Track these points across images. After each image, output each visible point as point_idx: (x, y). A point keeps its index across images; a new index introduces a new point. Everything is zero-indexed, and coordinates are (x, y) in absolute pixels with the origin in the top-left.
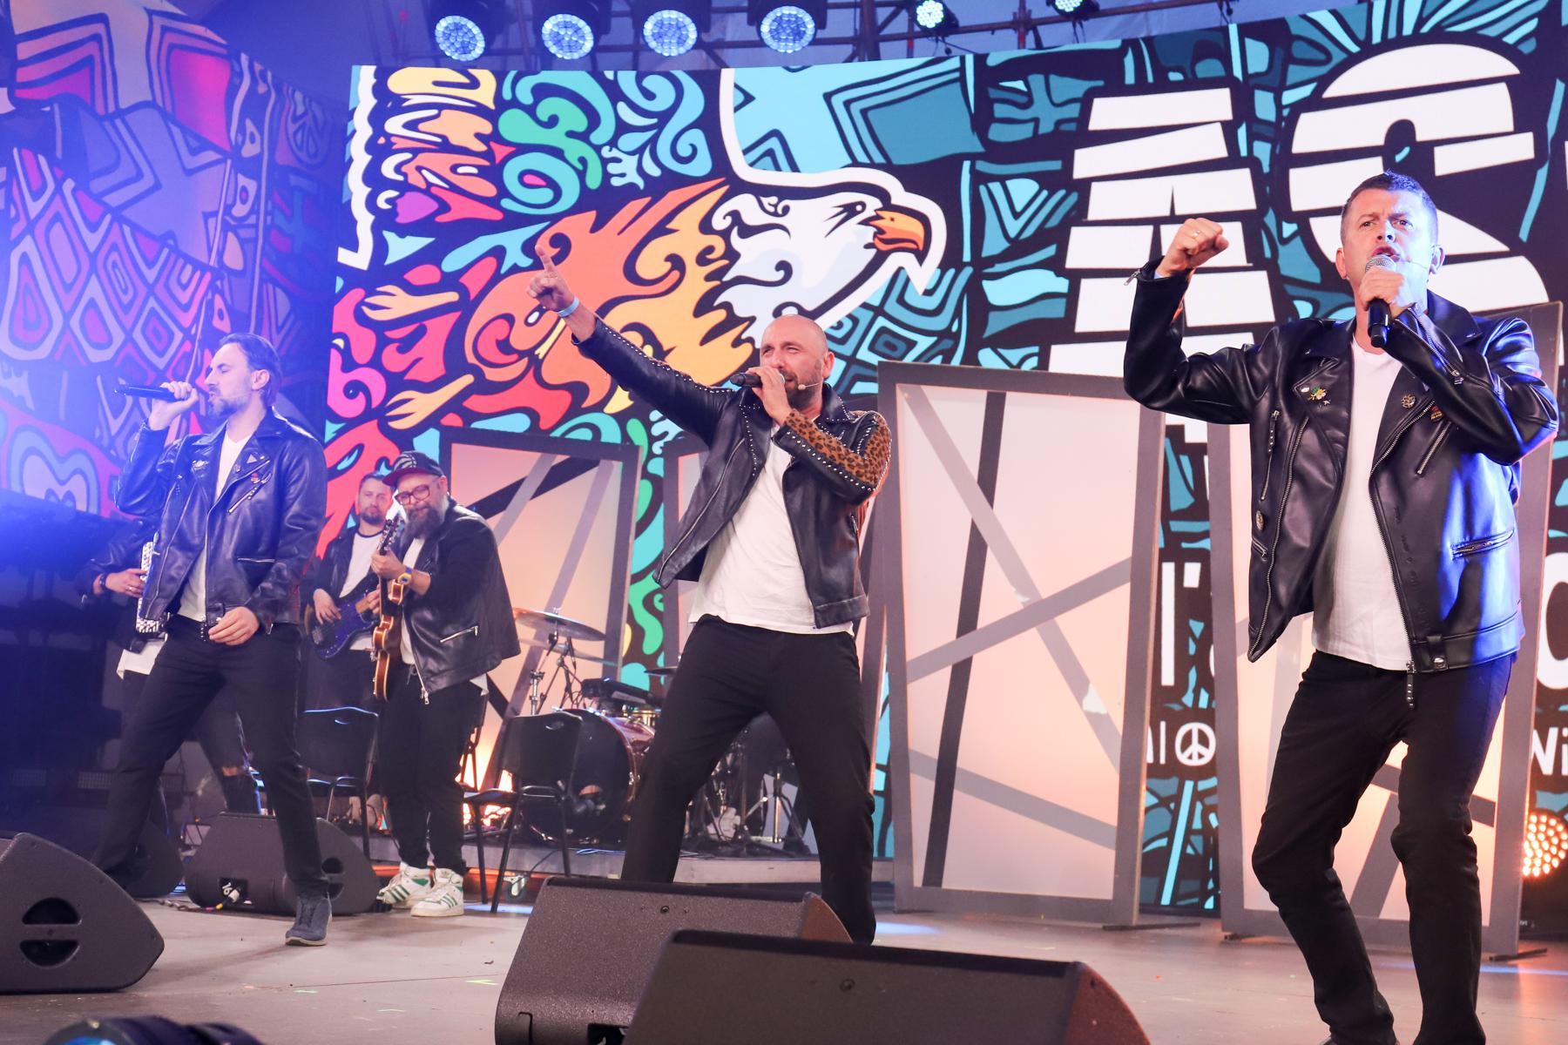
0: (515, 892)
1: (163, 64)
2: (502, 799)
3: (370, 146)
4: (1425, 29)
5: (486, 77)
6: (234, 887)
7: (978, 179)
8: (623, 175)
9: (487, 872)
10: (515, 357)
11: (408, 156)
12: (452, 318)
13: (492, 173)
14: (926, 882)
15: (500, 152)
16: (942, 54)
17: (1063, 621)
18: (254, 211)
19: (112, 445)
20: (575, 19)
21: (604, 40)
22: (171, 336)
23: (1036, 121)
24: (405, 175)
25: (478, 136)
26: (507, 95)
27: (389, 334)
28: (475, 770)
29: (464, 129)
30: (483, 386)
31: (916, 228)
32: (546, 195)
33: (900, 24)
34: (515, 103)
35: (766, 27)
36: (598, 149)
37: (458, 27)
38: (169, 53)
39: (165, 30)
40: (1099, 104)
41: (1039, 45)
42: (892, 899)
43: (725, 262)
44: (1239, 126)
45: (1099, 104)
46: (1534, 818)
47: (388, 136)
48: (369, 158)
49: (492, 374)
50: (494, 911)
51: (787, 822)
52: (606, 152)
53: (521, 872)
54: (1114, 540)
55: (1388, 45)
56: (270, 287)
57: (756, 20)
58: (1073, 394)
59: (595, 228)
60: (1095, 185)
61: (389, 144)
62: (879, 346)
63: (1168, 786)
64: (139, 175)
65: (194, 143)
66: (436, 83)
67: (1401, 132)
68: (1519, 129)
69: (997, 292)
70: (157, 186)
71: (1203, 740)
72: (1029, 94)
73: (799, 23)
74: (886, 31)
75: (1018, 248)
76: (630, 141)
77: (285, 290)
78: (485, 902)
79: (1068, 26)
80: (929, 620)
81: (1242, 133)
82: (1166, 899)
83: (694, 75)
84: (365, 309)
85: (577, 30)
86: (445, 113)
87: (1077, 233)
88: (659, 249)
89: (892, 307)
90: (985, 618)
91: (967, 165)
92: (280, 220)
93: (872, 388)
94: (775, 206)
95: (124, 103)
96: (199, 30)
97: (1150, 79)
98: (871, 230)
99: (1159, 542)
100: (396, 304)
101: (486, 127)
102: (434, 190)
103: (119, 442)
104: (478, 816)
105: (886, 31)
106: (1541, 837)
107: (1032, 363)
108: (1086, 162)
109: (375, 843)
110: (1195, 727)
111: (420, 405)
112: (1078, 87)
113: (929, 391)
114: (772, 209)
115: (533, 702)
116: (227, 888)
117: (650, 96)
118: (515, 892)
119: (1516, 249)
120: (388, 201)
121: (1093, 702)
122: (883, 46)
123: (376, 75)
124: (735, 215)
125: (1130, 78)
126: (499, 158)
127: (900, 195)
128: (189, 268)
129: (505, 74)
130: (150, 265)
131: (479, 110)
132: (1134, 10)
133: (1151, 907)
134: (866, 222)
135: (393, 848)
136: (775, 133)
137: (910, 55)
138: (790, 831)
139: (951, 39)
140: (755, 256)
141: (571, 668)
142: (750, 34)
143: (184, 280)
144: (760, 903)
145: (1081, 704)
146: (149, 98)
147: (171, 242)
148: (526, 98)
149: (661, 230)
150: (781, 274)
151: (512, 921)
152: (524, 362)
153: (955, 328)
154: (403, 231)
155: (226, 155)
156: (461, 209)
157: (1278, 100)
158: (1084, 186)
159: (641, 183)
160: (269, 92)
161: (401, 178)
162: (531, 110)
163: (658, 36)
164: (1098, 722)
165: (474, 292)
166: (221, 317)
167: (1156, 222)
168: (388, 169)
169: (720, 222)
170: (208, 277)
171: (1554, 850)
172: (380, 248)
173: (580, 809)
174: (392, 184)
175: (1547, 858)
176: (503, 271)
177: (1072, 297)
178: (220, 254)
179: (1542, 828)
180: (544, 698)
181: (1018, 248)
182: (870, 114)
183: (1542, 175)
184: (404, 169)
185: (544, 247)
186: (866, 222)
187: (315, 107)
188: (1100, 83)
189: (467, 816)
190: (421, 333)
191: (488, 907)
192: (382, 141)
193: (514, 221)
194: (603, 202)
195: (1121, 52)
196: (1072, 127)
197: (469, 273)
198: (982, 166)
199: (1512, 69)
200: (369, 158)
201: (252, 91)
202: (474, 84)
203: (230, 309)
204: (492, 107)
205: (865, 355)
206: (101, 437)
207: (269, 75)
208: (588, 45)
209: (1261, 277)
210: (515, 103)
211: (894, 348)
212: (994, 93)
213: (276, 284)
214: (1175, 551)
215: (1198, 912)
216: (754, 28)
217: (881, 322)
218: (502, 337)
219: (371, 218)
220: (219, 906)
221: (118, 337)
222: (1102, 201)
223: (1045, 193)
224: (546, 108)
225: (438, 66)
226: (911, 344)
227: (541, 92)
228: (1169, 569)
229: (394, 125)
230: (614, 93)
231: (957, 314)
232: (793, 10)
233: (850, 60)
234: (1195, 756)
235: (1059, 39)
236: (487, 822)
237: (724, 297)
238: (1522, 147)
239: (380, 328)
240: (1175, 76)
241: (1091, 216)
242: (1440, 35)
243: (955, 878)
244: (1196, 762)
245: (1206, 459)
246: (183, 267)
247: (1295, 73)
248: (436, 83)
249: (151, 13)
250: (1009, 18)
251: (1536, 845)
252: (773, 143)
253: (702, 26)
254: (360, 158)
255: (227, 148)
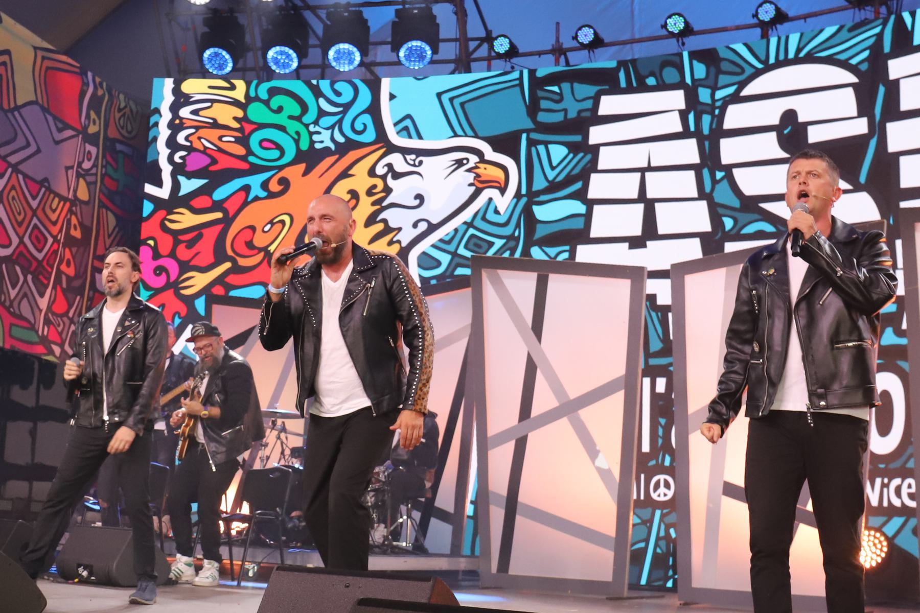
0: (251, 574)
1: (42, 78)
2: (243, 519)
3: (171, 125)
4: (802, 55)
5: (240, 84)
6: (85, 569)
7: (531, 143)
8: (322, 142)
9: (234, 562)
10: (256, 251)
11: (193, 131)
12: (219, 228)
13: (243, 141)
14: (499, 570)
15: (248, 128)
16: (508, 69)
17: (585, 414)
18: (95, 165)
19: (11, 305)
20: (286, 49)
21: (305, 62)
22: (46, 240)
23: (565, 111)
24: (191, 142)
25: (235, 119)
26: (252, 94)
27: (182, 238)
28: (227, 502)
29: (227, 115)
30: (237, 269)
31: (500, 174)
32: (275, 154)
33: (483, 51)
34: (257, 99)
35: (402, 53)
36: (307, 126)
37: (217, 55)
38: (46, 71)
39: (43, 58)
40: (604, 99)
41: (567, 64)
42: (478, 580)
43: (383, 194)
44: (689, 112)
45: (604, 99)
46: (866, 533)
47: (181, 119)
48: (170, 132)
49: (242, 262)
50: (239, 586)
51: (414, 534)
52: (312, 128)
53: (255, 563)
54: (613, 362)
55: (779, 64)
56: (104, 210)
57: (396, 49)
58: (590, 275)
59: (305, 174)
60: (602, 149)
61: (182, 123)
62: (471, 246)
63: (646, 513)
64: (28, 145)
65: (60, 125)
66: (210, 87)
67: (789, 116)
68: (860, 115)
69: (542, 212)
70: (38, 151)
71: (667, 485)
72: (561, 94)
73: (423, 51)
74: (475, 56)
75: (554, 187)
76: (326, 121)
77: (112, 211)
78: (233, 580)
79: (585, 52)
80: (502, 412)
81: (691, 117)
82: (643, 581)
83: (364, 81)
84: (167, 223)
85: (288, 56)
86: (215, 105)
87: (594, 176)
88: (341, 190)
89: (479, 223)
90: (535, 411)
91: (524, 136)
92: (110, 170)
93: (467, 271)
94: (414, 160)
95: (20, 102)
96: (64, 58)
97: (635, 84)
98: (473, 175)
99: (641, 365)
100: (185, 219)
101: (240, 113)
102: (209, 152)
103: (15, 304)
104: (228, 528)
105: (475, 56)
106: (871, 544)
107: (565, 255)
108: (596, 134)
109: (166, 545)
110: (662, 477)
111: (199, 281)
112: (591, 90)
113: (502, 273)
114: (412, 163)
115: (262, 460)
116: (80, 570)
117: (338, 94)
118: (251, 574)
119: (857, 188)
120: (181, 158)
121: (601, 462)
122: (473, 65)
123: (174, 82)
124: (390, 166)
125: (623, 84)
126: (247, 132)
127: (490, 154)
128: (57, 200)
129: (251, 82)
130: (34, 198)
131: (235, 103)
132: (624, 43)
133: (635, 586)
134: (469, 170)
135: (174, 545)
136: (408, 116)
137: (489, 70)
138: (416, 540)
139: (514, 60)
140: (401, 190)
141: (284, 440)
142: (392, 57)
143: (54, 206)
144: (405, 582)
145: (594, 463)
146: (34, 99)
147: (46, 184)
148: (264, 95)
149: (345, 175)
150: (417, 202)
151: (250, 591)
152: (262, 254)
153: (516, 234)
154: (189, 176)
155: (79, 132)
156: (224, 162)
157: (713, 95)
158: (596, 149)
159: (333, 147)
160: (104, 95)
161: (188, 144)
162: (266, 103)
163: (337, 59)
164: (604, 474)
165: (231, 213)
166: (75, 229)
167: (643, 171)
168: (181, 138)
169: (380, 170)
170: (68, 205)
171: (878, 552)
172: (176, 186)
173: (290, 525)
174: (183, 148)
175: (874, 556)
176: (249, 199)
177: (588, 216)
178: (75, 191)
179: (872, 538)
180: (268, 458)
181: (554, 187)
182: (466, 106)
183: (873, 143)
184: (190, 138)
185: (274, 187)
186: (469, 170)
187: (131, 103)
188: (607, 87)
189: (222, 529)
190: (200, 236)
191: (235, 583)
192: (177, 121)
193: (256, 170)
194: (310, 158)
195: (616, 70)
196: (588, 114)
197: (229, 201)
198: (535, 136)
199: (853, 79)
200: (170, 132)
201: (94, 95)
202: (233, 88)
203: (81, 224)
204: (243, 101)
205: (462, 251)
206: (5, 300)
207: (104, 84)
208: (295, 65)
209: (704, 204)
210: (257, 99)
211: (480, 247)
212: (540, 94)
213: (107, 209)
214: (652, 372)
215: (663, 589)
216: (395, 54)
217: (472, 231)
218: (248, 239)
219: (171, 168)
220: (76, 580)
221: (15, 241)
222: (606, 158)
223: (571, 156)
224: (276, 102)
225: (204, 77)
226: (491, 244)
227: (273, 92)
228: (647, 381)
229: (185, 112)
230: (317, 93)
231: (518, 225)
232: (419, 43)
233: (453, 73)
234: (662, 495)
235: (582, 61)
236: (234, 533)
237: (382, 216)
238: (860, 127)
239: (175, 233)
240: (651, 81)
241: (600, 167)
242: (811, 59)
243: (516, 568)
244: (662, 499)
245: (670, 315)
246: (53, 200)
247: (723, 79)
248: (210, 87)
249: (35, 48)
250: (549, 47)
251: (867, 549)
252: (407, 122)
253: (364, 53)
254: (164, 133)
255: (80, 128)
